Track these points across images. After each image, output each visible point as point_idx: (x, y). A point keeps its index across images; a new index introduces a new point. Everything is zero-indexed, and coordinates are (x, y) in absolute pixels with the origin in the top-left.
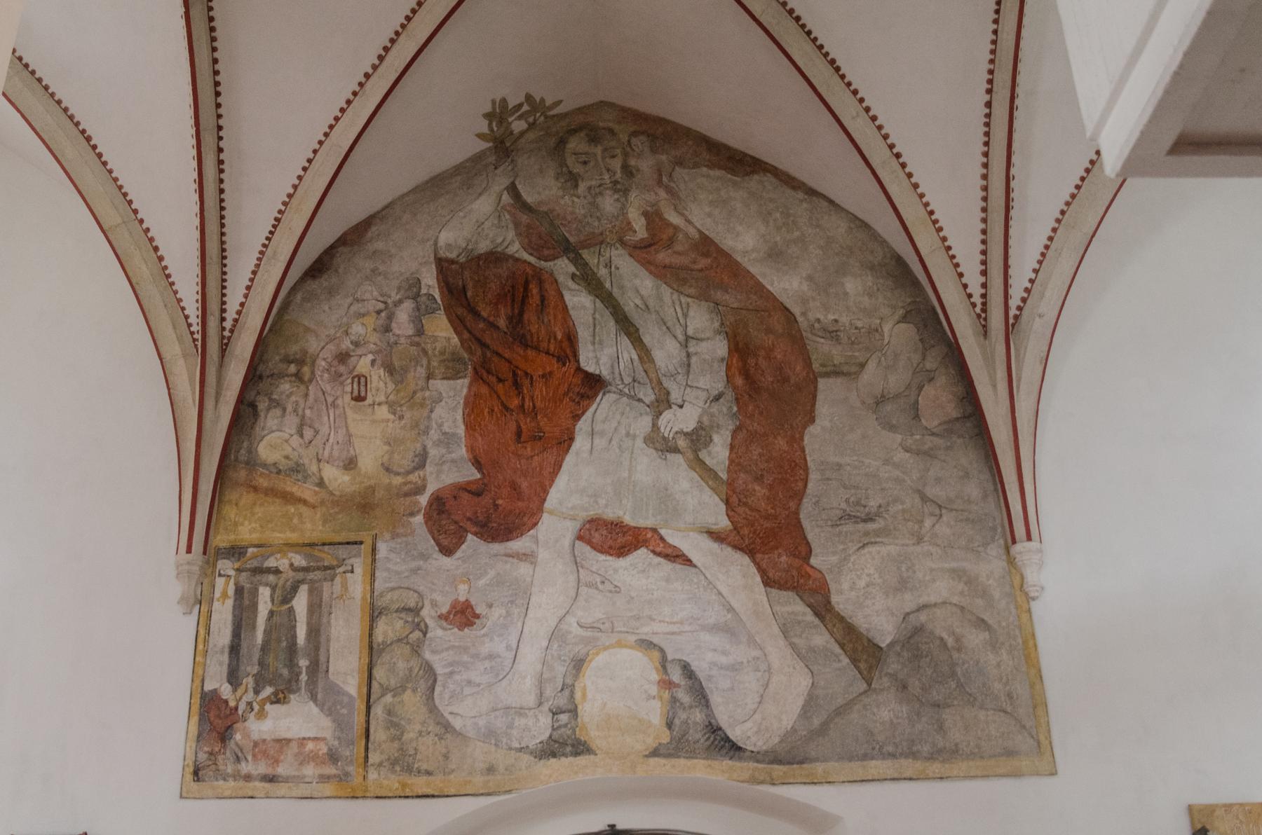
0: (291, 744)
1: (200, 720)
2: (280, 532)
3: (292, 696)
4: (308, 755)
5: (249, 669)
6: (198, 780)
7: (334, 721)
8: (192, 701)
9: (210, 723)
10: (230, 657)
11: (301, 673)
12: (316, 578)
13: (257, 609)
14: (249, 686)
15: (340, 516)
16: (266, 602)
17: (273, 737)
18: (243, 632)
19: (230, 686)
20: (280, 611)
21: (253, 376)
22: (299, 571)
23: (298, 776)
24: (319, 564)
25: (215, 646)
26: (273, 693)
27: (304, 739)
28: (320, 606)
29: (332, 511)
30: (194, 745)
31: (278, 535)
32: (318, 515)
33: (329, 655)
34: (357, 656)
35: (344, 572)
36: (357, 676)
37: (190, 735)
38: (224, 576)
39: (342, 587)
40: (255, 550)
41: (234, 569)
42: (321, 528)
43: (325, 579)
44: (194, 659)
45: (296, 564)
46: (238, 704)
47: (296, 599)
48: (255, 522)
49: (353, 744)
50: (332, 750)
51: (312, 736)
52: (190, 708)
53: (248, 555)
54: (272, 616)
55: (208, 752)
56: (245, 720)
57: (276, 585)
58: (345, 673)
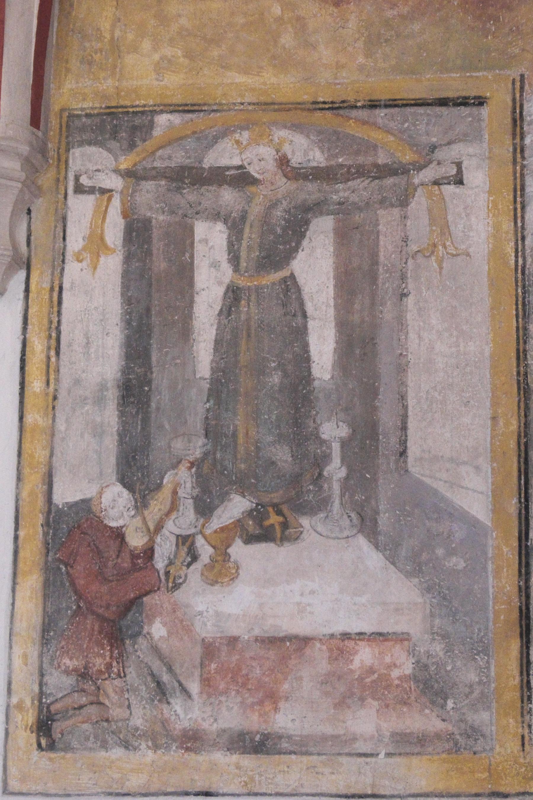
0: (308, 651)
1: (46, 584)
2: (246, 72)
3: (305, 521)
4: (361, 679)
5: (178, 445)
6: (52, 747)
7: (429, 590)
8: (22, 533)
9: (76, 592)
10: (122, 414)
11: (327, 458)
12: (354, 198)
13: (191, 283)
14: (181, 493)
15: (416, 27)
16: (215, 265)
17: (257, 632)
18: (154, 343)
19: (125, 493)
20: (258, 289)
21: (48, 366)
22: (305, 177)
23: (337, 737)
24: (361, 160)
25: (77, 382)
26: (249, 513)
27: (346, 636)
28: (373, 278)
29: (390, 13)
30: (34, 652)
31: (240, 79)
32: (353, 23)
33: (405, 408)
34: (486, 412)
35: (437, 183)
36: (486, 467)
37: (21, 626)
38: (91, 190)
39: (433, 221)
40: (176, 119)
41: (116, 171)
42: (361, 59)
43: (382, 202)
44: (21, 418)
45: (296, 160)
46: (152, 540)
47: (301, 255)
48: (172, 42)
49: (485, 651)
50: (426, 667)
51: (367, 628)
52: (16, 553)
53: (157, 132)
54: (237, 300)
55: (75, 670)
56: (176, 586)
57: (243, 218)
58: (452, 460)
